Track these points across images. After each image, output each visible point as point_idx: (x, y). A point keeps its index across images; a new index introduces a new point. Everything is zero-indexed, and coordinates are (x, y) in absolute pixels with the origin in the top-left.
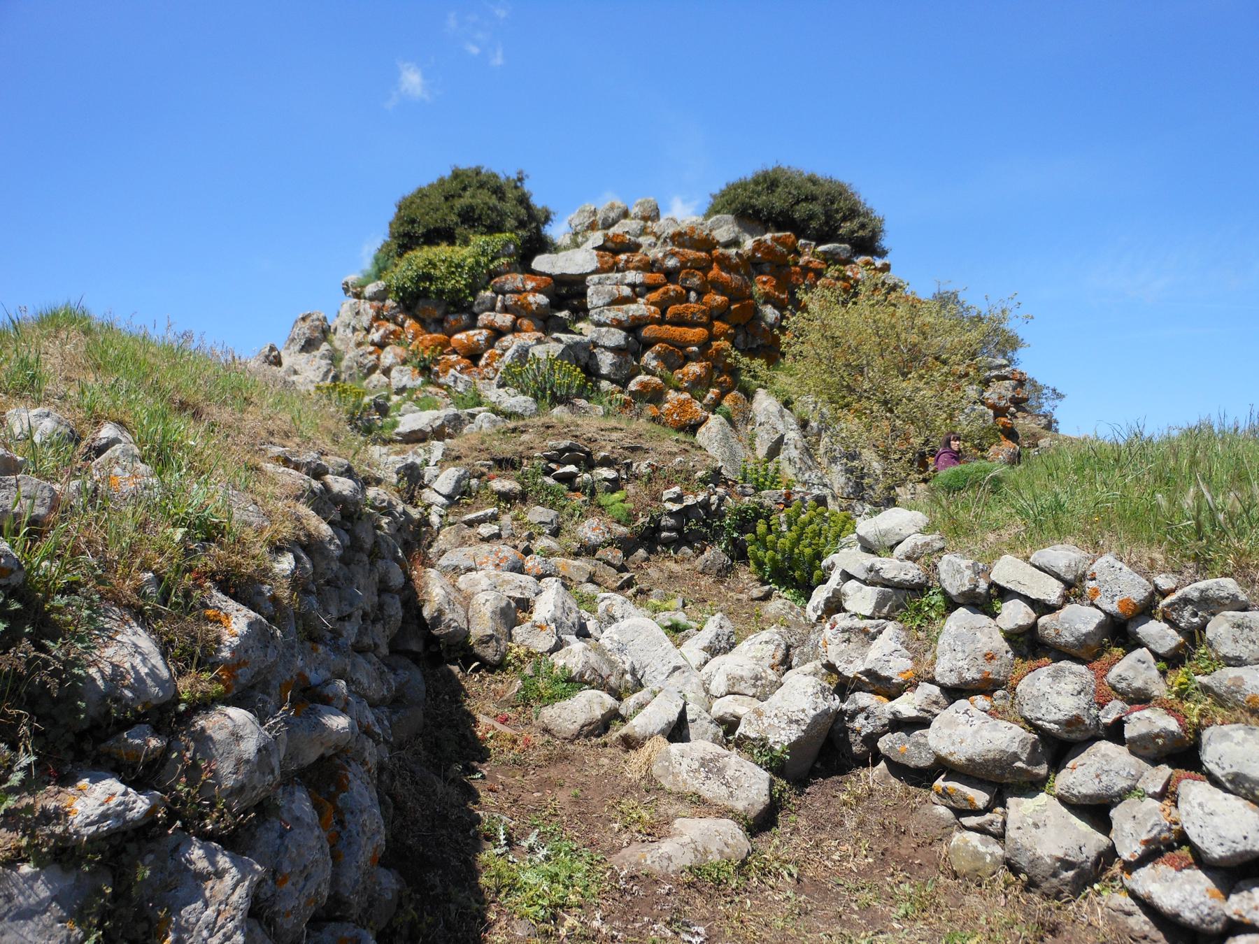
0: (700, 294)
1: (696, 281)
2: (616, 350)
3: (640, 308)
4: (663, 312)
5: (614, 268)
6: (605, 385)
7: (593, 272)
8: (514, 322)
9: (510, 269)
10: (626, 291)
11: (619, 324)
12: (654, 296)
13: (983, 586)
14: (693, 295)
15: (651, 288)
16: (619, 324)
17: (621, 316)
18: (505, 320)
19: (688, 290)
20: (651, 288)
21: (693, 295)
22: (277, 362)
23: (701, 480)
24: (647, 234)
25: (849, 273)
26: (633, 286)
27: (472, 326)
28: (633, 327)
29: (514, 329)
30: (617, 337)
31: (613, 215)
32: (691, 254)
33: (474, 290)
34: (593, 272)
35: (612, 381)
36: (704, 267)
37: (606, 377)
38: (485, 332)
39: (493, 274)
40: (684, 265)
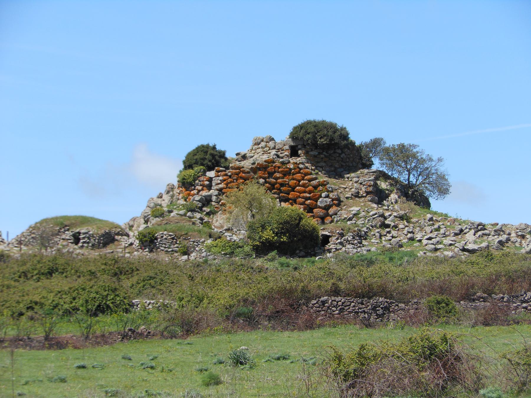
0: (237, 180)
1: (235, 178)
2: (216, 196)
3: (221, 186)
4: (227, 186)
5: (218, 176)
6: (213, 203)
7: (215, 177)
8: (202, 188)
9: (202, 175)
10: (219, 182)
11: (217, 190)
12: (225, 182)
13: (211, 216)
14: (235, 181)
15: (225, 180)
16: (217, 190)
17: (218, 188)
18: (200, 188)
19: (234, 180)
20: (225, 180)
21: (235, 181)
22: (161, 197)
23: (330, 252)
24: (267, 147)
25: (288, 166)
26: (220, 180)
27: (194, 189)
28: (220, 190)
29: (202, 190)
30: (216, 192)
31: (259, 141)
32: (234, 171)
33: (194, 180)
34: (215, 177)
35: (216, 202)
36: (237, 174)
37: (214, 202)
38: (197, 191)
39: (199, 177)
40: (232, 174)
